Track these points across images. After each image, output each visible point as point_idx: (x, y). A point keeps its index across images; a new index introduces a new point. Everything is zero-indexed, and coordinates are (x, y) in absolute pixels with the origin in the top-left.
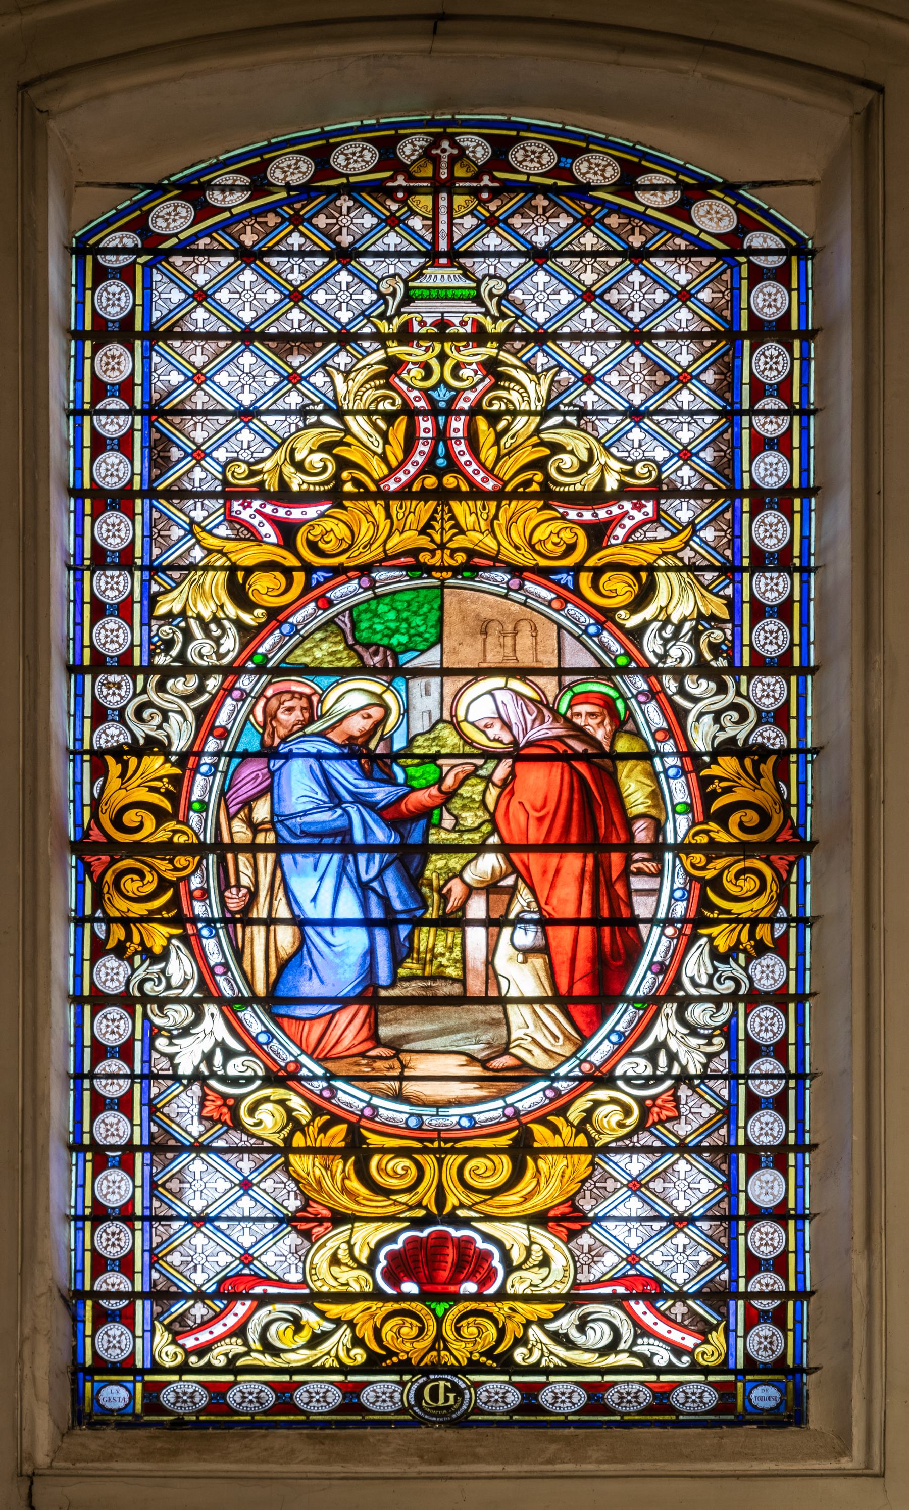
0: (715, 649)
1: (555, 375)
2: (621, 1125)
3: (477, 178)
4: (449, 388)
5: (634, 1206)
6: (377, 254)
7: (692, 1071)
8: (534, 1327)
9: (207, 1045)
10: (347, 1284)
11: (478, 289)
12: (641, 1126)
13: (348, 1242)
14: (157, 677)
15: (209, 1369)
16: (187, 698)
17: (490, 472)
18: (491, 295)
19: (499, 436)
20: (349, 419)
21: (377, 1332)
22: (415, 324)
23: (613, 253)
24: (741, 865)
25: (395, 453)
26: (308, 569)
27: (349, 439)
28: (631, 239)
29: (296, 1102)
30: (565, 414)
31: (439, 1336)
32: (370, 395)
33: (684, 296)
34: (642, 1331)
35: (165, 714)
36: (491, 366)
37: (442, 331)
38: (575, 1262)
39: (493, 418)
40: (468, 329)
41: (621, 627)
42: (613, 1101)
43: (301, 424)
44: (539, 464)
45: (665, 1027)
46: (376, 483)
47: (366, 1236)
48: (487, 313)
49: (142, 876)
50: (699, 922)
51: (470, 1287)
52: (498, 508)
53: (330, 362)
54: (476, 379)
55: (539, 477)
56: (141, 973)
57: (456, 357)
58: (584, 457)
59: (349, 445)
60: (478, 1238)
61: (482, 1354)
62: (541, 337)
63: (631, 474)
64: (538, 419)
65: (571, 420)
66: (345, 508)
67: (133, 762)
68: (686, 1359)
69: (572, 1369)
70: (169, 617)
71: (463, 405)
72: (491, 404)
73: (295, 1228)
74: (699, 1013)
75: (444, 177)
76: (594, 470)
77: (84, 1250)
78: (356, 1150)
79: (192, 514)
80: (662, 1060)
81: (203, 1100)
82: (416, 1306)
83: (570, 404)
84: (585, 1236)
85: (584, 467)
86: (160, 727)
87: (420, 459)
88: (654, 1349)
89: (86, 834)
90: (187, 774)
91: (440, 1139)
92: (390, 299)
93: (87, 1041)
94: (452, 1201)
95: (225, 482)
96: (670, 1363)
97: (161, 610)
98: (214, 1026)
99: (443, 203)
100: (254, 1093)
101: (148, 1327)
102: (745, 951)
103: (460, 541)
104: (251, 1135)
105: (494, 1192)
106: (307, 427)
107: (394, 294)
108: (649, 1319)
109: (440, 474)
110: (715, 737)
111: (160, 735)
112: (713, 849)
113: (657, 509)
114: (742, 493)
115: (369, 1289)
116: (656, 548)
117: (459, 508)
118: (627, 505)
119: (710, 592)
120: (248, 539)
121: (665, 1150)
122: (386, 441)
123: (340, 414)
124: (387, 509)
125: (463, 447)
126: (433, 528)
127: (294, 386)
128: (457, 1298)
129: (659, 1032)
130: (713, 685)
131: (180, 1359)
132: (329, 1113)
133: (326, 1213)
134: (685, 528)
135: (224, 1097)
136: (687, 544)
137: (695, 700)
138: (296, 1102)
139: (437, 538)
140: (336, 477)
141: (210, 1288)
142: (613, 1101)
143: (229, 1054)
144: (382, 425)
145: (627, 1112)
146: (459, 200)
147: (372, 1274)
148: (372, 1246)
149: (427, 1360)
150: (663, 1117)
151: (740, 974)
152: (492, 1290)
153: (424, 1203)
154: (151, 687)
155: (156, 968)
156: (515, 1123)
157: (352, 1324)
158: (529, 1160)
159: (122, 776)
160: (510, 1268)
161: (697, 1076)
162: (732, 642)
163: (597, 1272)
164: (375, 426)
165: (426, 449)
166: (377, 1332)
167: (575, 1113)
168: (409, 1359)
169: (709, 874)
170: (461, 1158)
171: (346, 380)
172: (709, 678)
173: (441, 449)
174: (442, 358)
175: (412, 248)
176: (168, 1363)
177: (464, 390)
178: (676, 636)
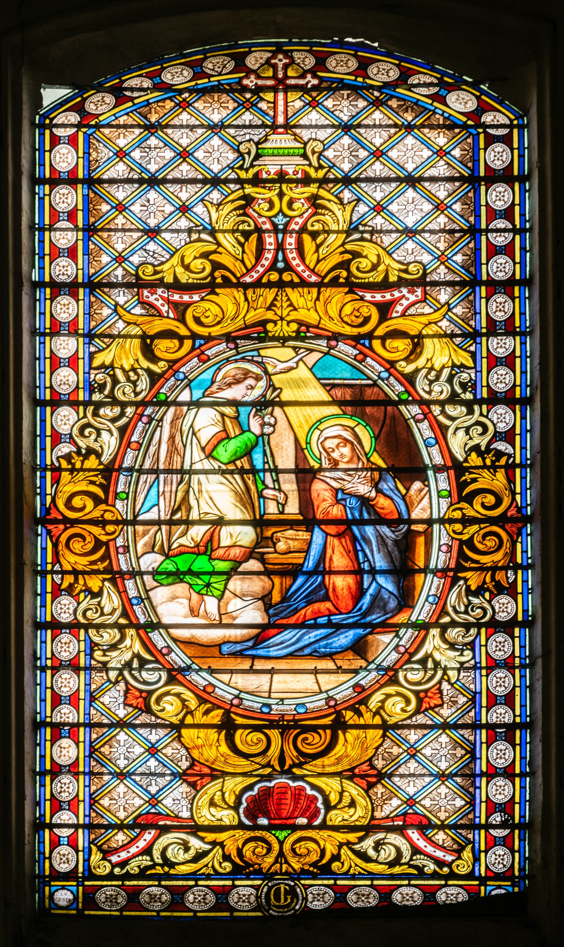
0: (463, 386)
1: (355, 206)
2: (403, 710)
4: (285, 216)
6: (237, 127)
8: (345, 847)
9: (127, 656)
10: (221, 820)
11: (304, 148)
12: (417, 712)
13: (221, 790)
14: (92, 408)
16: (113, 420)
17: (313, 271)
18: (314, 152)
19: (318, 247)
20: (220, 236)
21: (240, 852)
22: (264, 173)
25: (250, 260)
26: (194, 336)
27: (220, 249)
31: (281, 854)
33: (441, 153)
34: (416, 851)
37: (282, 178)
38: (372, 804)
39: (314, 235)
42: (398, 694)
43: (188, 240)
44: (345, 265)
45: (433, 642)
47: (233, 785)
48: (310, 165)
49: (84, 539)
50: (460, 568)
51: (303, 821)
52: (319, 293)
54: (303, 209)
55: (344, 274)
56: (83, 606)
58: (375, 261)
59: (221, 253)
60: (308, 788)
61: (311, 865)
62: (347, 181)
63: (406, 271)
65: (367, 236)
66: (217, 294)
68: (446, 870)
69: (372, 876)
70: (103, 366)
71: (293, 226)
73: (185, 781)
76: (382, 268)
78: (228, 727)
79: (117, 299)
81: (127, 691)
84: (379, 786)
87: (266, 263)
88: (425, 862)
92: (246, 156)
95: (137, 276)
97: (96, 363)
102: (488, 589)
103: (294, 315)
104: (157, 717)
106: (191, 242)
107: (249, 153)
109: (281, 272)
110: (466, 444)
111: (96, 446)
113: (425, 293)
114: (481, 283)
116: (424, 320)
117: (294, 295)
118: (405, 291)
119: (461, 348)
123: (213, 232)
124: (245, 294)
125: (294, 255)
126: (276, 306)
128: (295, 828)
129: (428, 647)
130: (464, 409)
131: (108, 871)
132: (211, 702)
133: (206, 771)
135: (141, 691)
137: (453, 419)
138: (188, 695)
139: (279, 313)
140: (212, 274)
142: (398, 694)
144: (242, 240)
145: (408, 702)
148: (237, 793)
150: (432, 705)
151: (486, 605)
152: (317, 822)
153: (272, 763)
154: (89, 415)
157: (222, 845)
160: (329, 807)
163: (387, 810)
166: (240, 852)
167: (374, 702)
169: (465, 537)
173: (280, 257)
174: (281, 195)
177: (295, 217)
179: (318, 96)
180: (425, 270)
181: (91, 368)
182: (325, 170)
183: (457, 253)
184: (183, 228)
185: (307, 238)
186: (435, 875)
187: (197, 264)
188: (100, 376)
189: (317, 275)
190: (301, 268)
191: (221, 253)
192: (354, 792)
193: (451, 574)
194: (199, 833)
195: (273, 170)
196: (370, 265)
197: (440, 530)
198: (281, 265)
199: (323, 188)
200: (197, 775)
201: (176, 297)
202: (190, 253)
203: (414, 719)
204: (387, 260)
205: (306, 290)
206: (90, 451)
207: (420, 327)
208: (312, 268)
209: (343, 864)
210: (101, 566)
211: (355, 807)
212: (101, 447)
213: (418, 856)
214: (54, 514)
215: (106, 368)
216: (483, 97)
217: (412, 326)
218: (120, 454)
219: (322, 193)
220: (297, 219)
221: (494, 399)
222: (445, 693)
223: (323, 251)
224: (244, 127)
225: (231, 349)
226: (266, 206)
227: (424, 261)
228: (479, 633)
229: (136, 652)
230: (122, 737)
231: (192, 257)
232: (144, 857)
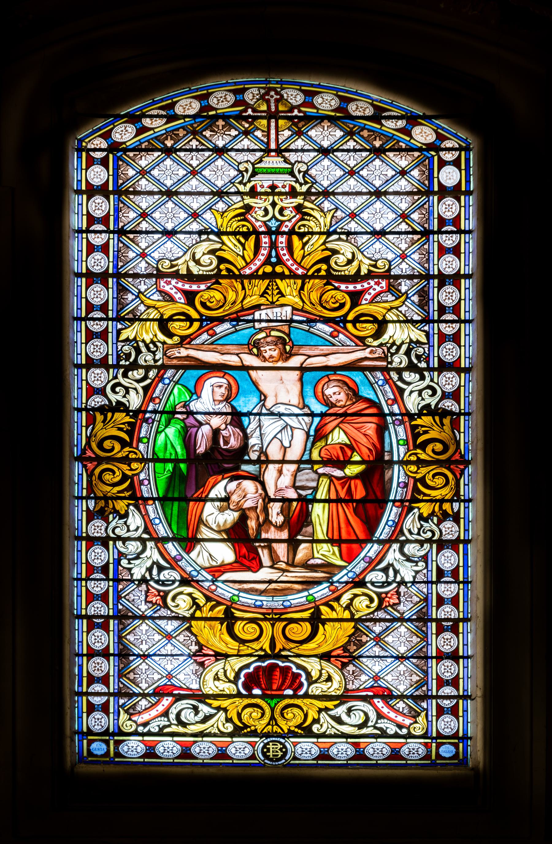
0: (418, 357)
1: (335, 213)
2: (368, 607)
4: (277, 220)
5: (377, 650)
6: (237, 150)
9: (149, 564)
10: (224, 691)
11: (292, 168)
12: (379, 608)
13: (224, 668)
14: (123, 370)
15: (149, 734)
16: (138, 381)
17: (299, 264)
18: (300, 172)
19: (304, 245)
21: (239, 715)
23: (365, 150)
24: (434, 472)
25: (249, 253)
27: (224, 247)
28: (374, 143)
29: (197, 595)
32: (235, 225)
34: (380, 716)
35: (127, 389)
36: (299, 208)
38: (345, 679)
40: (287, 189)
43: (198, 240)
44: (326, 260)
46: (239, 270)
47: (236, 663)
48: (297, 181)
51: (290, 692)
53: (214, 207)
55: (324, 267)
56: (113, 524)
57: (280, 204)
58: (350, 257)
59: (224, 251)
61: (296, 727)
62: (326, 194)
63: (375, 266)
64: (325, 236)
65: (344, 237)
66: (220, 284)
67: (109, 415)
70: (127, 340)
71: (284, 229)
72: (299, 228)
74: (410, 549)
75: (273, 110)
76: (355, 263)
78: (229, 619)
80: (391, 572)
81: (147, 591)
82: (259, 701)
83: (342, 228)
85: (350, 262)
87: (262, 258)
88: (387, 725)
90: (139, 421)
91: (272, 613)
92: (245, 173)
93: (85, 674)
94: (279, 646)
95: (157, 269)
96: (396, 732)
97: (123, 337)
98: (152, 554)
99: (273, 124)
100: (175, 589)
105: (302, 642)
106: (201, 241)
108: (385, 710)
109: (274, 265)
111: (124, 400)
112: (420, 463)
116: (387, 305)
120: (170, 301)
121: (394, 620)
122: (244, 249)
126: (268, 294)
127: (195, 219)
130: (418, 376)
132: (215, 600)
134: (403, 295)
136: (404, 303)
137: (409, 384)
138: (197, 595)
139: (270, 300)
140: (218, 266)
141: (150, 690)
143: (161, 569)
145: (372, 600)
146: (281, 122)
147: (237, 685)
148: (236, 670)
149: (265, 730)
151: (435, 528)
152: (301, 693)
154: (120, 376)
155: (122, 521)
156: (313, 605)
157: (225, 710)
158: (321, 626)
159: (104, 421)
160: (311, 682)
161: (410, 582)
163: (357, 684)
164: (239, 241)
166: (239, 715)
168: (256, 730)
170: (285, 623)
173: (274, 253)
174: (274, 204)
175: (256, 147)
179: (303, 126)
181: (118, 341)
183: (414, 252)
184: (194, 230)
185: (295, 238)
186: (396, 736)
187: (206, 259)
188: (126, 348)
190: (289, 263)
191: (224, 251)
192: (331, 671)
193: (407, 504)
194: (207, 701)
195: (266, 184)
197: (399, 471)
198: (274, 260)
204: (360, 256)
205: (292, 281)
209: (321, 726)
210: (127, 494)
211: (332, 681)
212: (128, 401)
213: (382, 720)
214: (89, 453)
217: (378, 310)
219: (307, 204)
220: (287, 223)
221: (443, 367)
224: (243, 150)
226: (262, 213)
227: (389, 258)
228: (431, 547)
229: (155, 561)
231: (202, 253)
232: (163, 718)
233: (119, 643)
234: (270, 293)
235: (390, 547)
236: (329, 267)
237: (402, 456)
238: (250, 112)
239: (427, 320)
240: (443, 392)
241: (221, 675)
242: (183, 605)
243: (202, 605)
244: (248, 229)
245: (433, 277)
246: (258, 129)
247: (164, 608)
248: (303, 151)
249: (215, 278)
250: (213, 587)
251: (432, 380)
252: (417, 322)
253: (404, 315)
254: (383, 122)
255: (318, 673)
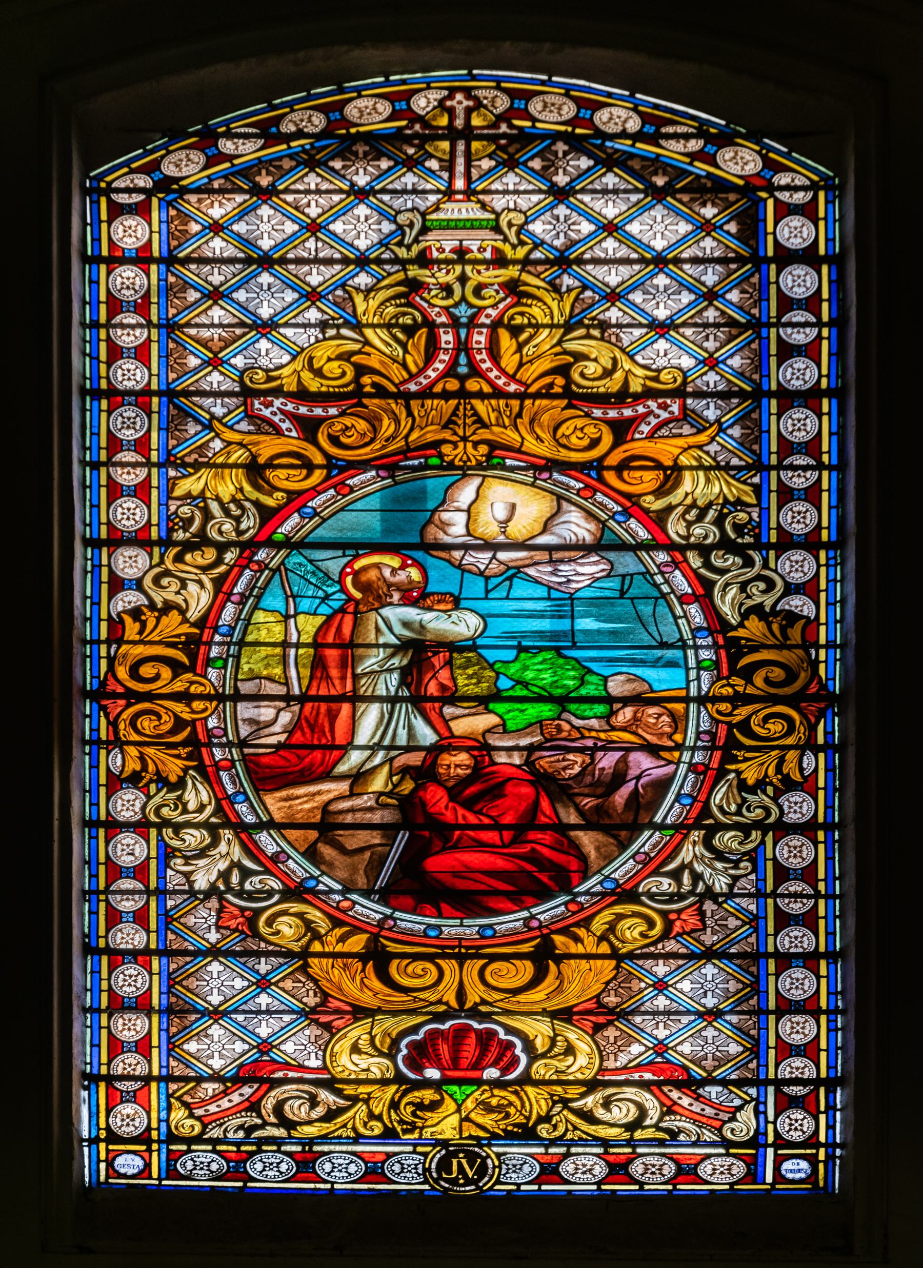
2: (643, 935)
3: (495, 125)
4: (470, 306)
6: (394, 192)
7: (717, 889)
9: (223, 865)
11: (497, 220)
12: (666, 935)
16: (205, 569)
17: (512, 378)
18: (510, 225)
20: (369, 332)
28: (654, 179)
29: (315, 915)
30: (588, 327)
32: (391, 310)
36: (512, 288)
38: (600, 1052)
40: (488, 255)
41: (647, 511)
42: (635, 914)
43: (320, 336)
44: (563, 370)
48: (506, 240)
49: (159, 717)
51: (492, 1073)
53: (350, 282)
56: (157, 800)
57: (475, 278)
63: (656, 379)
65: (596, 333)
70: (188, 496)
71: (483, 320)
74: (727, 840)
76: (619, 375)
77: (826, 219)
80: (686, 878)
81: (220, 911)
85: (608, 373)
86: (178, 593)
89: (103, 684)
92: (407, 230)
94: (472, 998)
97: (178, 492)
98: (229, 848)
101: (164, 1104)
103: (484, 434)
105: (516, 992)
106: (325, 339)
107: (411, 225)
110: (742, 604)
111: (179, 600)
115: (390, 1075)
117: (481, 407)
123: (358, 327)
125: (484, 356)
126: (456, 423)
129: (686, 854)
132: (348, 924)
134: (711, 425)
135: (242, 909)
136: (713, 439)
137: (722, 572)
138: (315, 915)
139: (461, 433)
142: (635, 914)
143: (246, 873)
144: (400, 336)
145: (651, 924)
146: (475, 145)
156: (537, 933)
161: (722, 895)
162: (759, 523)
163: (623, 1059)
165: (447, 358)
167: (599, 924)
170: (482, 962)
171: (366, 299)
172: (735, 554)
174: (463, 279)
176: (185, 1132)
178: (700, 518)
179: (518, 151)
180: (685, 377)
182: (526, 248)
188: (185, 509)
189: (519, 382)
195: (448, 245)
196: (600, 371)
197: (699, 713)
199: (529, 272)
200: (325, 1015)
201: (303, 410)
202: (321, 354)
203: (660, 946)
205: (502, 402)
206: (168, 607)
207: (677, 451)
208: (511, 372)
212: (185, 601)
215: (195, 498)
216: (771, 155)
218: (215, 609)
219: (525, 277)
221: (786, 542)
222: (709, 914)
223: (528, 350)
224: (404, 191)
225: (383, 479)
230: (215, 967)
233: (169, 992)
234: (460, 422)
235: (686, 836)
236: (569, 381)
237: (705, 688)
238: (417, 127)
239: (759, 466)
240: (787, 585)
241: (364, 1043)
242: (288, 930)
243: (323, 932)
244: (414, 319)
245: (770, 394)
246: (431, 156)
247: (253, 937)
248: (516, 192)
249: (352, 398)
250: (346, 904)
251: (766, 566)
252: (739, 469)
253: (714, 459)
254: (663, 142)
255: (548, 1042)
